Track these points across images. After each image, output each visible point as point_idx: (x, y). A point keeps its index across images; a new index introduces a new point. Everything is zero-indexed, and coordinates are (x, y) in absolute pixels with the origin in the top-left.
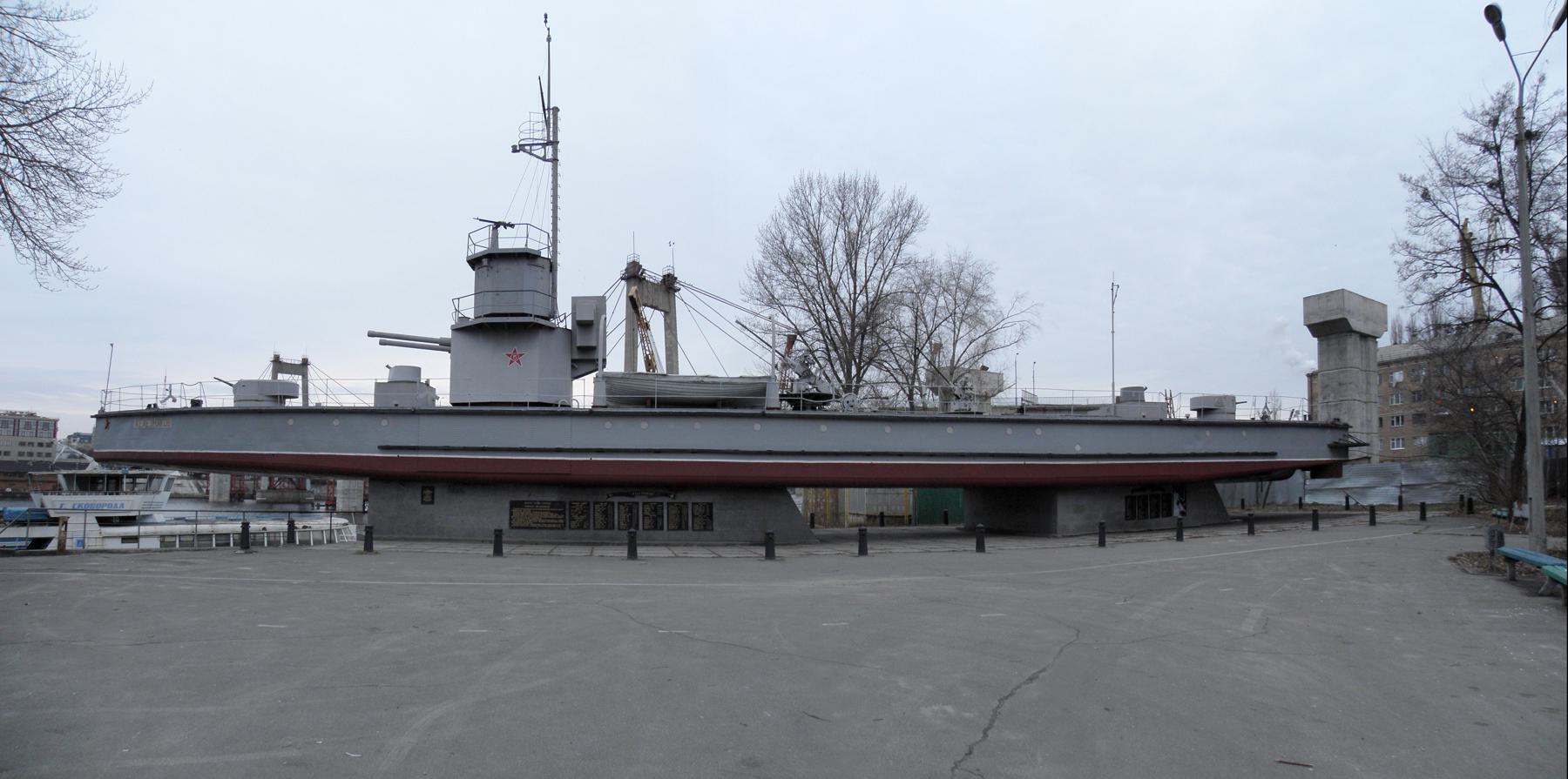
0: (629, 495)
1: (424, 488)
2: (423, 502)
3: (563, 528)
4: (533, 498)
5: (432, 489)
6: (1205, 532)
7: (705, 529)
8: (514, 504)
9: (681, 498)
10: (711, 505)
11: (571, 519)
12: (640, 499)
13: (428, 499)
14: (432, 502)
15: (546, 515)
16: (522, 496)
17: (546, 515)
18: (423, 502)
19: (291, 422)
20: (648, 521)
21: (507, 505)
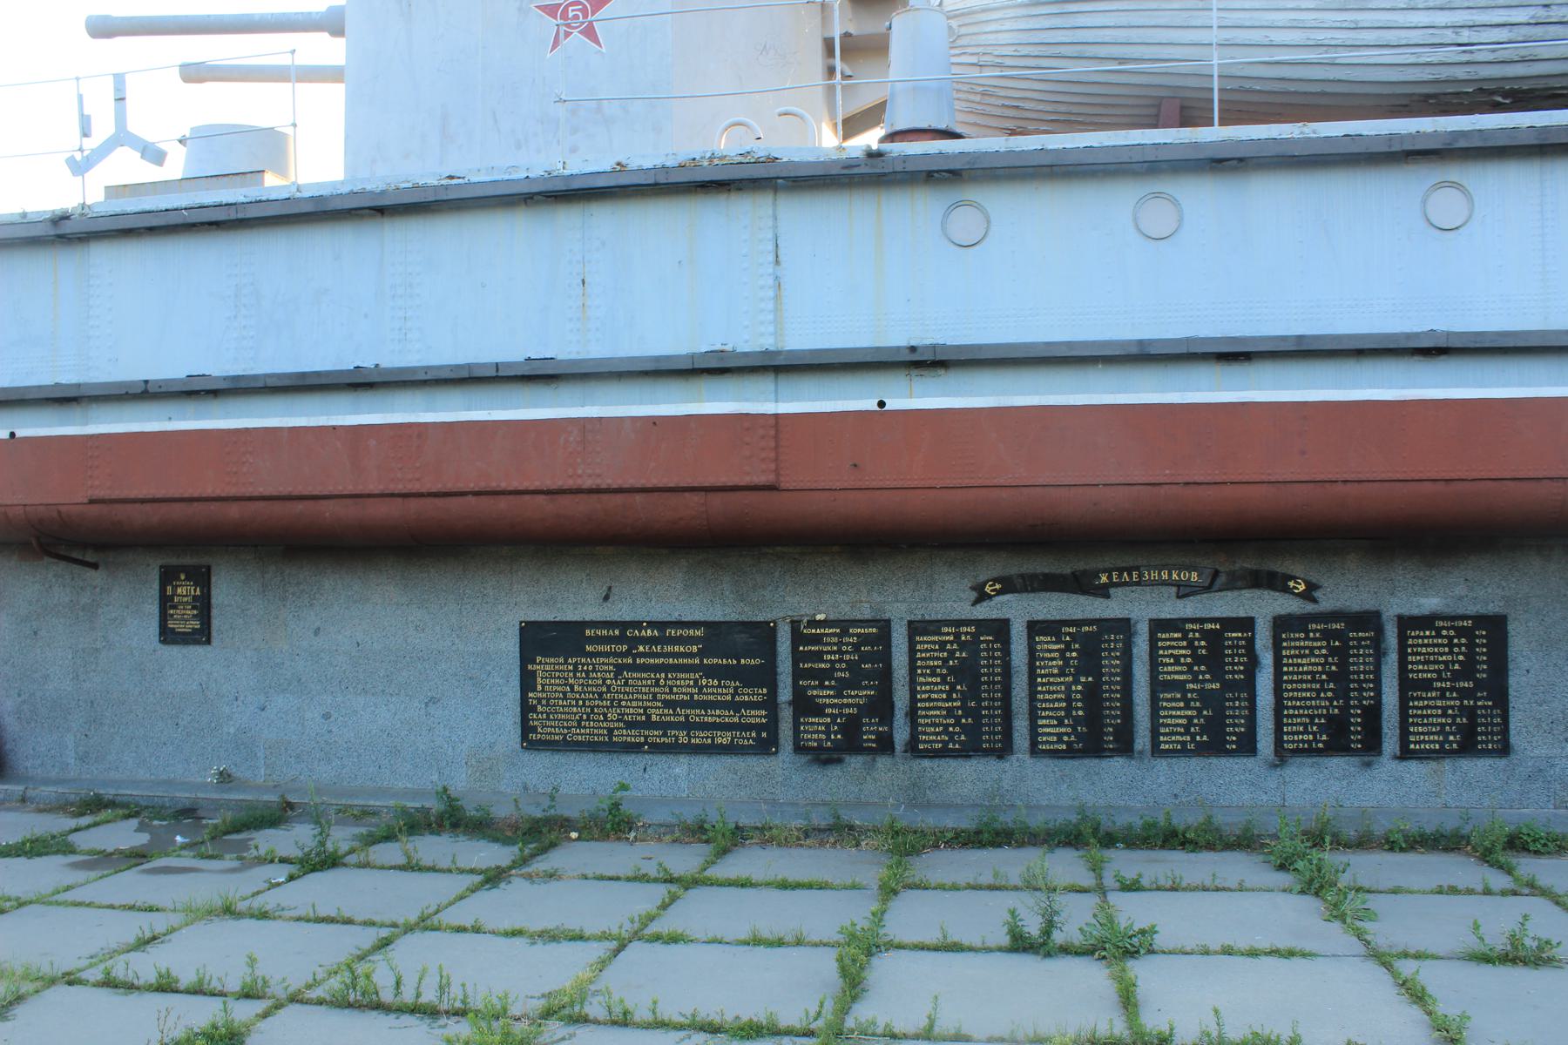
0: (1081, 584)
1: (168, 576)
2: (168, 636)
3: (766, 745)
4: (621, 610)
5: (202, 578)
6: (1043, 594)
7: (1468, 746)
8: (539, 640)
9: (1347, 589)
10: (1496, 626)
11: (804, 706)
12: (1139, 605)
13: (184, 620)
14: (202, 635)
15: (684, 686)
16: (576, 599)
17: (684, 686)
18: (168, 636)
19: (400, 486)
20: (1176, 714)
21: (510, 646)
